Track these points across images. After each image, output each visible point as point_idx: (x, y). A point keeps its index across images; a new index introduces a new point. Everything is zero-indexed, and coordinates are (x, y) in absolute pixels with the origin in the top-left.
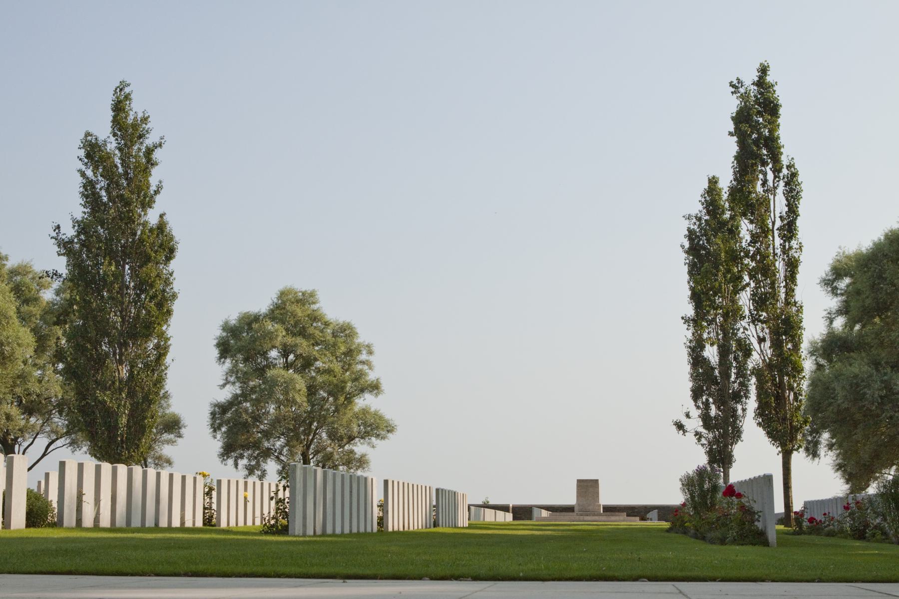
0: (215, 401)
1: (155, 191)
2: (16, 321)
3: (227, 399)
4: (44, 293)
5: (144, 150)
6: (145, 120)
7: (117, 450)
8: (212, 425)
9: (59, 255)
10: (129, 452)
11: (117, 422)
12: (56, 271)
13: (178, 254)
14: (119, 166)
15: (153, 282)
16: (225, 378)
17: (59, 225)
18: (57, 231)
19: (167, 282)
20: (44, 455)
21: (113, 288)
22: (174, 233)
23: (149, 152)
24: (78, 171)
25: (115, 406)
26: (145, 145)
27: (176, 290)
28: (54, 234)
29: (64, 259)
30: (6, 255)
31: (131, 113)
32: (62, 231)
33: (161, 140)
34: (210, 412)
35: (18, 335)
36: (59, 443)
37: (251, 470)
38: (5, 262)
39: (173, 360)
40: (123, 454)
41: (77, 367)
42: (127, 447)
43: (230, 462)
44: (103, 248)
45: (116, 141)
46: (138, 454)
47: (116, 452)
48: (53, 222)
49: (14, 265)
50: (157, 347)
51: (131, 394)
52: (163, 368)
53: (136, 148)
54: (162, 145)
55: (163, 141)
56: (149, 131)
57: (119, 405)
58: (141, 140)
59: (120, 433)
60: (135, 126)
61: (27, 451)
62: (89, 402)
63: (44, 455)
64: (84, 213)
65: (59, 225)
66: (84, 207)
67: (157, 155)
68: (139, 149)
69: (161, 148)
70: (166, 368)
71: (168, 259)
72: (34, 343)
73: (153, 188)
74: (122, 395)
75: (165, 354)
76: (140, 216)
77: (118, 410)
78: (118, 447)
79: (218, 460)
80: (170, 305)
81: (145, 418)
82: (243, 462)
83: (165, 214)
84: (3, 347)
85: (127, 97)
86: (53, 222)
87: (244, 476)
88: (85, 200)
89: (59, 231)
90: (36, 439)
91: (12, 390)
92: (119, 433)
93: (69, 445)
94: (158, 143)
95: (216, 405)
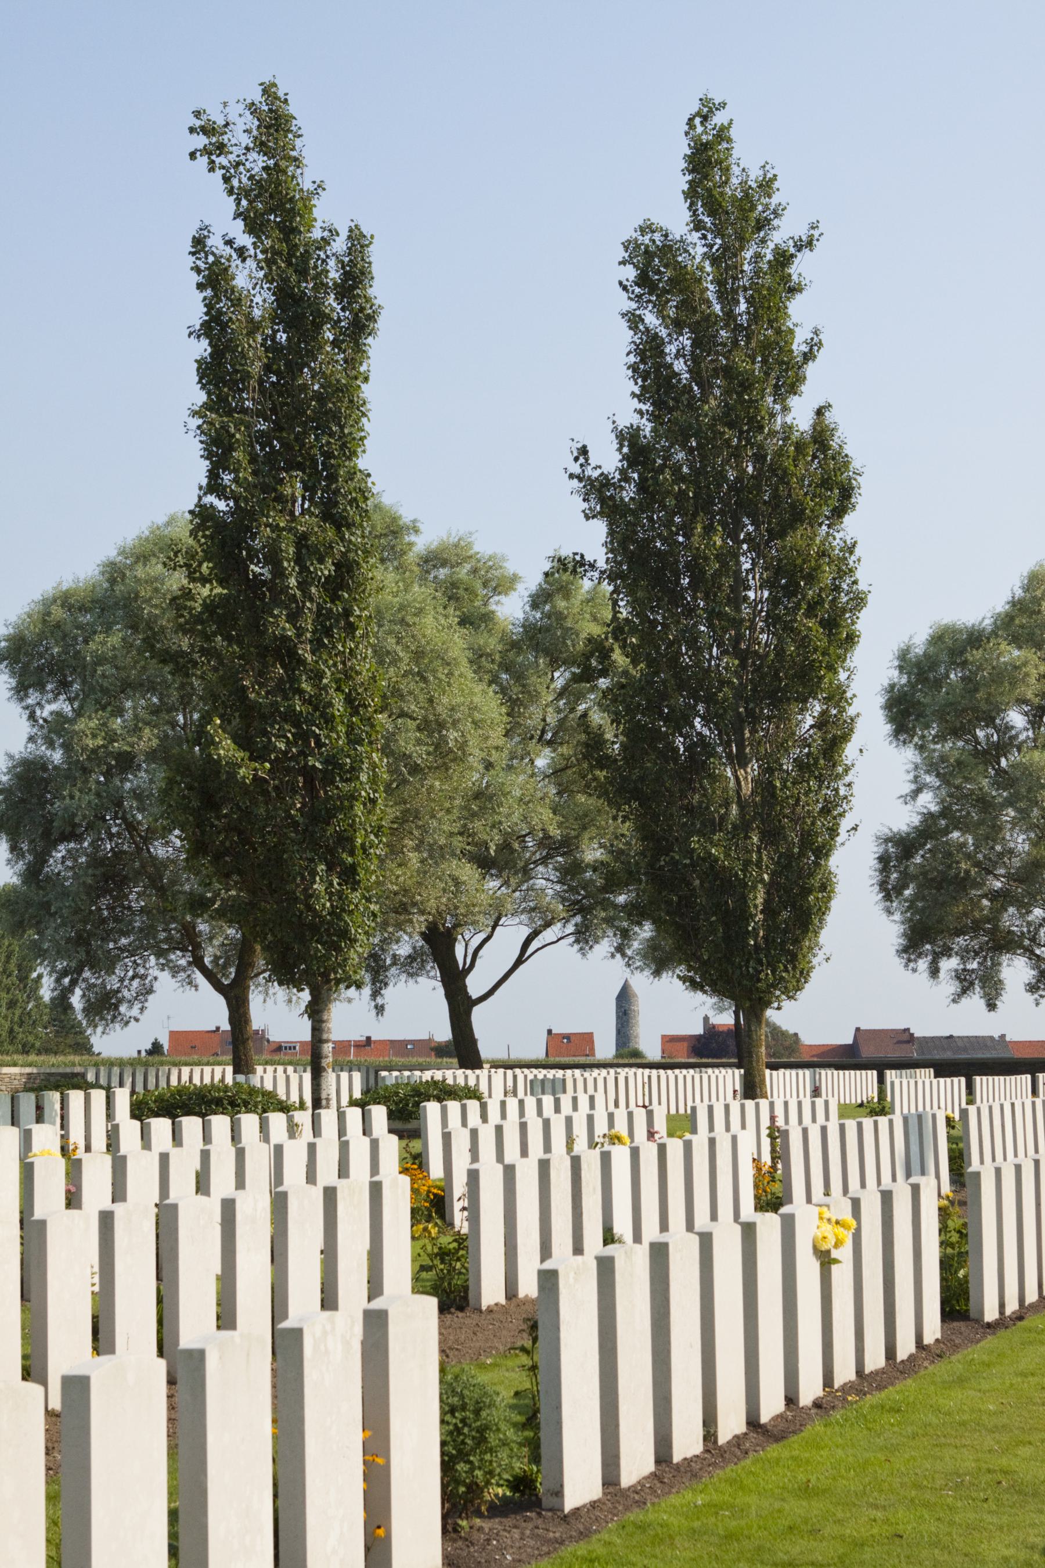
0: (887, 831)
1: (805, 354)
2: (465, 668)
3: (913, 825)
4: (498, 603)
5: (769, 257)
6: (767, 185)
7: (747, 967)
8: (883, 885)
9: (587, 517)
10: (773, 972)
11: (746, 902)
12: (582, 556)
13: (865, 500)
14: (714, 302)
15: (815, 570)
16: (911, 776)
17: (584, 447)
18: (582, 460)
19: (844, 570)
20: (519, 962)
21: (719, 588)
22: (848, 450)
23: (783, 259)
24: (623, 315)
25: (738, 867)
26: (771, 245)
27: (862, 586)
28: (576, 469)
29: (599, 528)
30: (414, 521)
31: (735, 170)
32: (593, 462)
33: (812, 232)
34: (877, 855)
35: (472, 702)
36: (549, 935)
37: (965, 983)
38: (413, 538)
39: (861, 751)
40: (762, 976)
41: (642, 779)
42: (770, 959)
43: (923, 964)
44: (691, 494)
45: (703, 242)
46: (794, 976)
47: (745, 972)
48: (573, 440)
49: (431, 543)
50: (822, 723)
51: (772, 836)
52: (840, 769)
53: (748, 254)
54: (815, 242)
55: (816, 233)
56: (780, 212)
57: (747, 863)
58: (762, 234)
59: (754, 928)
60: (746, 202)
61: (481, 953)
62: (677, 857)
63: (519, 962)
64: (640, 412)
65: (584, 447)
66: (640, 401)
67: (801, 267)
68: (758, 256)
69: (811, 250)
70: (847, 770)
71: (839, 513)
72: (505, 719)
73: (798, 346)
74: (750, 838)
75: (845, 737)
76: (772, 415)
77: (745, 875)
78: (748, 961)
79: (898, 963)
80: (849, 621)
81: (810, 891)
82: (949, 964)
83: (830, 406)
84: (444, 732)
85: (722, 134)
86: (573, 440)
87: (952, 997)
88: (639, 381)
89: (587, 460)
90: (498, 928)
91: (465, 825)
92: (750, 928)
93: (572, 939)
94: (804, 238)
95: (887, 840)
